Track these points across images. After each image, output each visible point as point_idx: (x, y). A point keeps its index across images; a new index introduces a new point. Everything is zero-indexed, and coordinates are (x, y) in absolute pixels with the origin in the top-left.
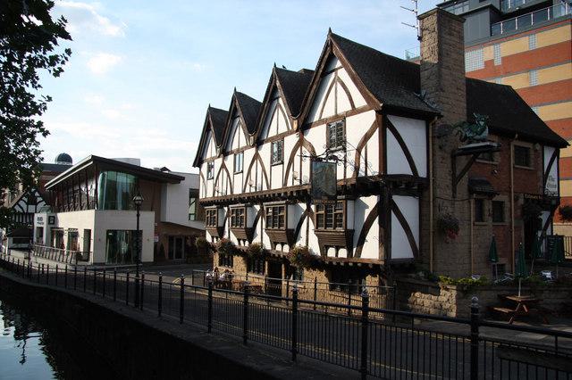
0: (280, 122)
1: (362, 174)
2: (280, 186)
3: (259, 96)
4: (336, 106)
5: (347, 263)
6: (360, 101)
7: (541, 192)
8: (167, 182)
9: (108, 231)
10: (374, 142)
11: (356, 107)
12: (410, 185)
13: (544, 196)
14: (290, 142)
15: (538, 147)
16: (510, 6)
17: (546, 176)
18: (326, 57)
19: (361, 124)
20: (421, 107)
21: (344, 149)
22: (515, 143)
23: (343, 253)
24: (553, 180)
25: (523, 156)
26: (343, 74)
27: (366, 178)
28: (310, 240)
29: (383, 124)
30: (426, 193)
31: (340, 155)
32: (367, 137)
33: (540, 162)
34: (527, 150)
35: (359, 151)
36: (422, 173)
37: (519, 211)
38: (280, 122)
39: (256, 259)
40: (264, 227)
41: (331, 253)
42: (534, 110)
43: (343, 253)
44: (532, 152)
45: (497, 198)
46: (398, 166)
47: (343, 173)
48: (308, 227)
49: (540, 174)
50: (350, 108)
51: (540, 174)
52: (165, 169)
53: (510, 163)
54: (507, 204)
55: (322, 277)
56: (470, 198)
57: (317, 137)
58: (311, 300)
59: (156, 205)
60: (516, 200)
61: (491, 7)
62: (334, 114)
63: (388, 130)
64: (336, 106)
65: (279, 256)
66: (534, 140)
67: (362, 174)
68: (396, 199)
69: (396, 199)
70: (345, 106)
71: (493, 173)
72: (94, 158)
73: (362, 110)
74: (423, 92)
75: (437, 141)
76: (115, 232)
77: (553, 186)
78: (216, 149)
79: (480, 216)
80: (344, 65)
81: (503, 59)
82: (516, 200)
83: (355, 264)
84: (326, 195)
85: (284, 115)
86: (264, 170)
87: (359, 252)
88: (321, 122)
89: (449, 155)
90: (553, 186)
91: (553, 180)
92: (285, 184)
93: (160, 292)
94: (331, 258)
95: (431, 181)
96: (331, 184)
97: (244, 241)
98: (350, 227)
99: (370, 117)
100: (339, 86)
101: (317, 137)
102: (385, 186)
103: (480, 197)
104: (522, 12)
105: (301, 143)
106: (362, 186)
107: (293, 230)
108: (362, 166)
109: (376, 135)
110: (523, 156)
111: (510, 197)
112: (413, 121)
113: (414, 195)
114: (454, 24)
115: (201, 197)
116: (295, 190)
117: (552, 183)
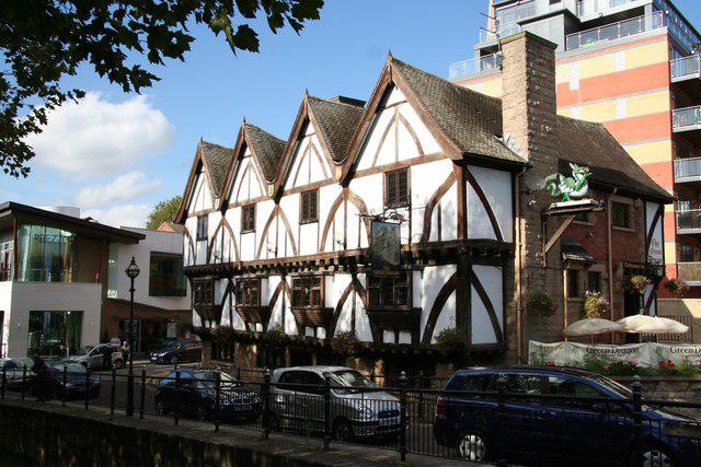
0: (313, 164)
1: (433, 238)
3: (283, 133)
4: (397, 151)
5: (24, 393)
6: (432, 145)
7: (643, 261)
8: (109, 242)
9: (32, 313)
11: (426, 154)
13: (647, 264)
14: (328, 196)
15: (639, 202)
16: (587, 15)
17: (648, 240)
18: (384, 87)
20: (505, 155)
21: (409, 206)
22: (613, 198)
23: (405, 338)
25: (622, 215)
26: (408, 111)
27: (440, 243)
31: (403, 211)
32: (441, 192)
33: (641, 221)
34: (626, 206)
36: (507, 238)
37: (618, 284)
38: (313, 164)
40: (234, 303)
41: (389, 338)
42: (626, 148)
44: (632, 210)
45: (594, 268)
46: (480, 229)
47: (410, 234)
48: (231, 304)
49: (642, 237)
50: (417, 155)
51: (642, 237)
52: (90, 218)
53: (607, 224)
54: (604, 275)
57: (370, 191)
59: (102, 276)
60: (615, 270)
61: (566, 13)
64: (397, 151)
66: (634, 195)
67: (433, 238)
68: (477, 269)
69: (477, 269)
71: (588, 236)
72: (11, 203)
73: (432, 158)
76: (41, 314)
77: (657, 252)
78: (214, 198)
80: (409, 100)
81: (581, 82)
82: (615, 270)
83: (424, 352)
84: (389, 265)
85: (321, 160)
88: (373, 170)
90: (657, 252)
93: (113, 403)
94: (388, 345)
96: (394, 250)
99: (446, 167)
100: (401, 126)
103: (576, 267)
104: (602, 21)
106: (434, 253)
108: (434, 229)
110: (622, 215)
111: (608, 267)
112: (497, 172)
113: (496, 265)
114: (544, 52)
115: (185, 265)
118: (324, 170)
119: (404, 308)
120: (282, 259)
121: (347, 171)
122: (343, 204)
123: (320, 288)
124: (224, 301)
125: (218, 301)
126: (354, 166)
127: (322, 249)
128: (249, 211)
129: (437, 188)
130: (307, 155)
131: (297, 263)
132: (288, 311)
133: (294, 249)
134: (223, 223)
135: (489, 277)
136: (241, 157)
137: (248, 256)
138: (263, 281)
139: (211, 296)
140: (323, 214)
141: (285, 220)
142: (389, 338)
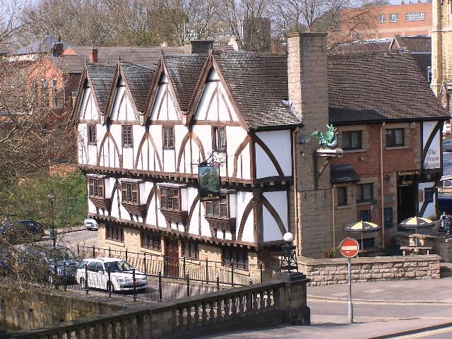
2: (173, 171)
5: (232, 245)
6: (236, 118)
10: (246, 153)
12: (281, 183)
13: (423, 169)
17: (424, 152)
19: (236, 136)
23: (229, 236)
24: (434, 153)
28: (200, 226)
29: (253, 137)
30: (291, 188)
31: (221, 155)
32: (242, 147)
35: (236, 156)
39: (150, 237)
41: (220, 235)
43: (229, 236)
46: (266, 170)
49: (417, 150)
55: (216, 257)
56: (331, 188)
58: (102, 288)
62: (217, 120)
63: (256, 144)
65: (175, 234)
68: (266, 195)
69: (266, 195)
70: (224, 118)
74: (290, 101)
75: (298, 146)
79: (343, 201)
83: (238, 245)
86: (156, 152)
87: (240, 235)
89: (311, 156)
91: (434, 153)
92: (98, 164)
95: (295, 179)
97: (137, 216)
98: (232, 216)
101: (203, 133)
102: (259, 187)
105: (189, 136)
107: (187, 212)
109: (248, 148)
111: (380, 177)
116: (187, 177)
117: (431, 156)
118: (120, 107)
119: (225, 218)
120: (238, 180)
121: (189, 120)
122: (189, 142)
123: (137, 191)
124: (113, 194)
125: (108, 195)
126: (194, 116)
127: (178, 170)
128: (168, 129)
129: (239, 145)
130: (166, 97)
131: (184, 179)
132: (203, 218)
133: (161, 167)
134: (108, 134)
135: (277, 199)
136: (119, 86)
137: (169, 168)
138: (141, 185)
139: (136, 197)
140: (178, 145)
141: (152, 140)
142: (220, 235)
